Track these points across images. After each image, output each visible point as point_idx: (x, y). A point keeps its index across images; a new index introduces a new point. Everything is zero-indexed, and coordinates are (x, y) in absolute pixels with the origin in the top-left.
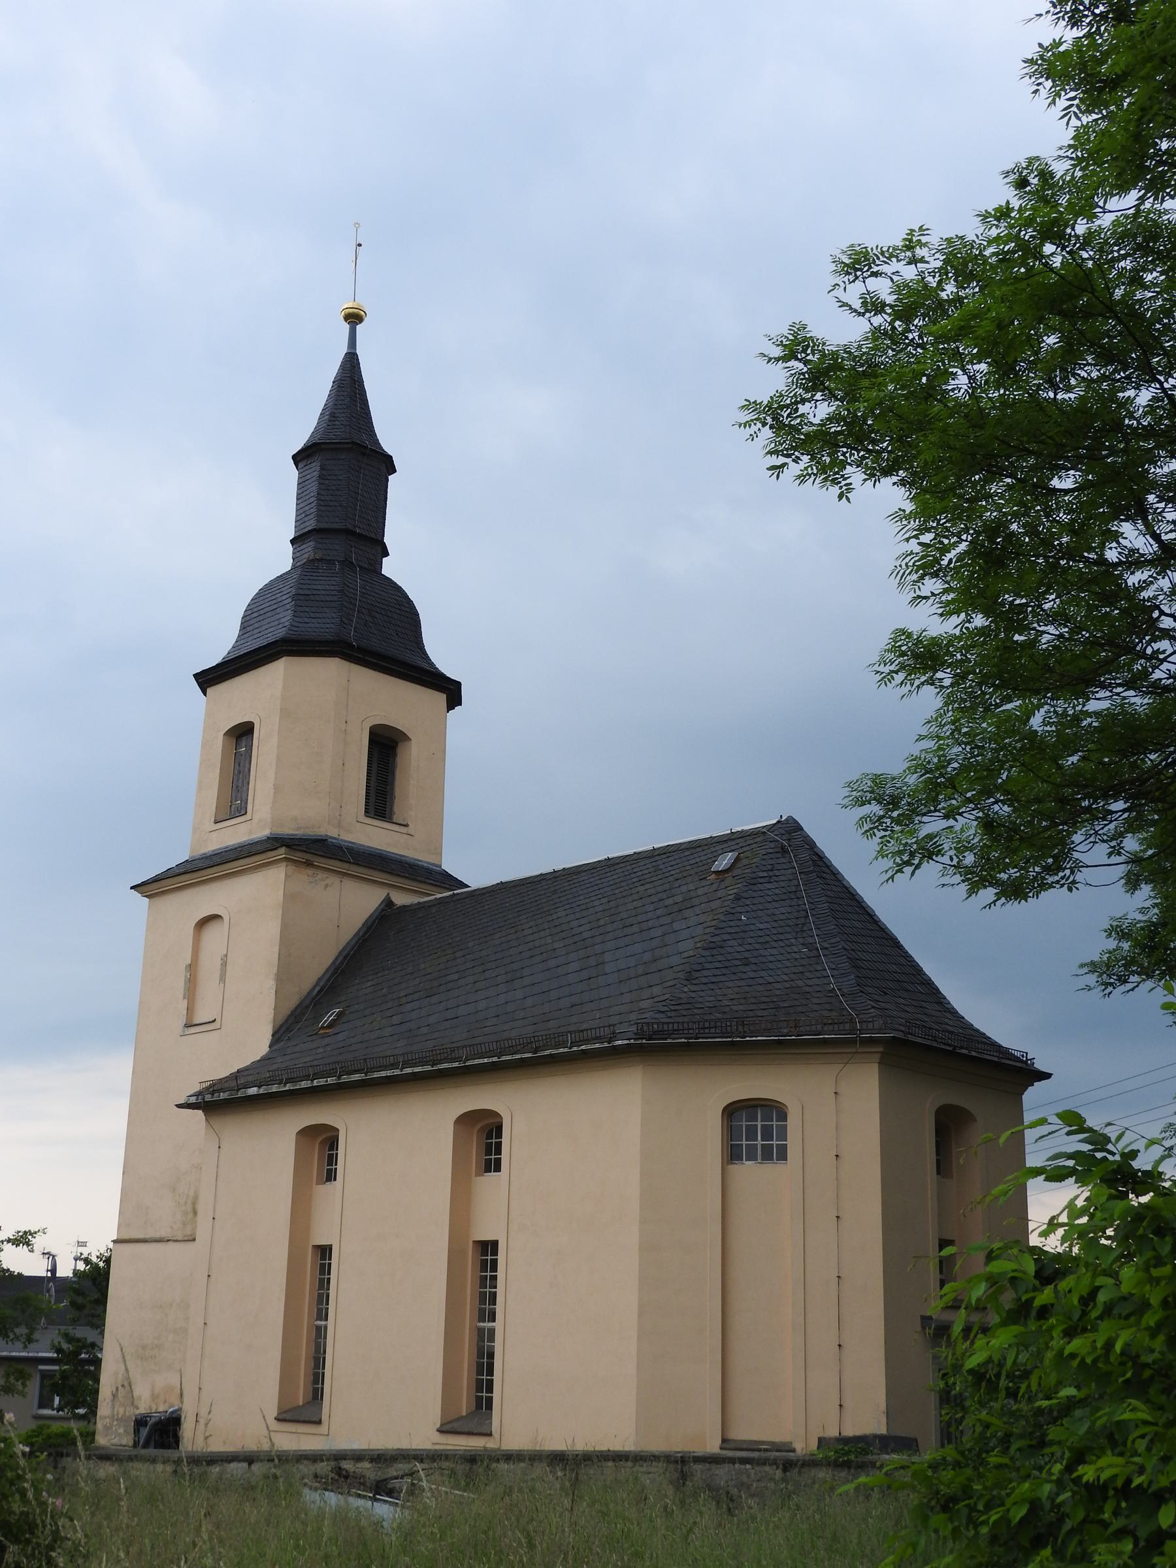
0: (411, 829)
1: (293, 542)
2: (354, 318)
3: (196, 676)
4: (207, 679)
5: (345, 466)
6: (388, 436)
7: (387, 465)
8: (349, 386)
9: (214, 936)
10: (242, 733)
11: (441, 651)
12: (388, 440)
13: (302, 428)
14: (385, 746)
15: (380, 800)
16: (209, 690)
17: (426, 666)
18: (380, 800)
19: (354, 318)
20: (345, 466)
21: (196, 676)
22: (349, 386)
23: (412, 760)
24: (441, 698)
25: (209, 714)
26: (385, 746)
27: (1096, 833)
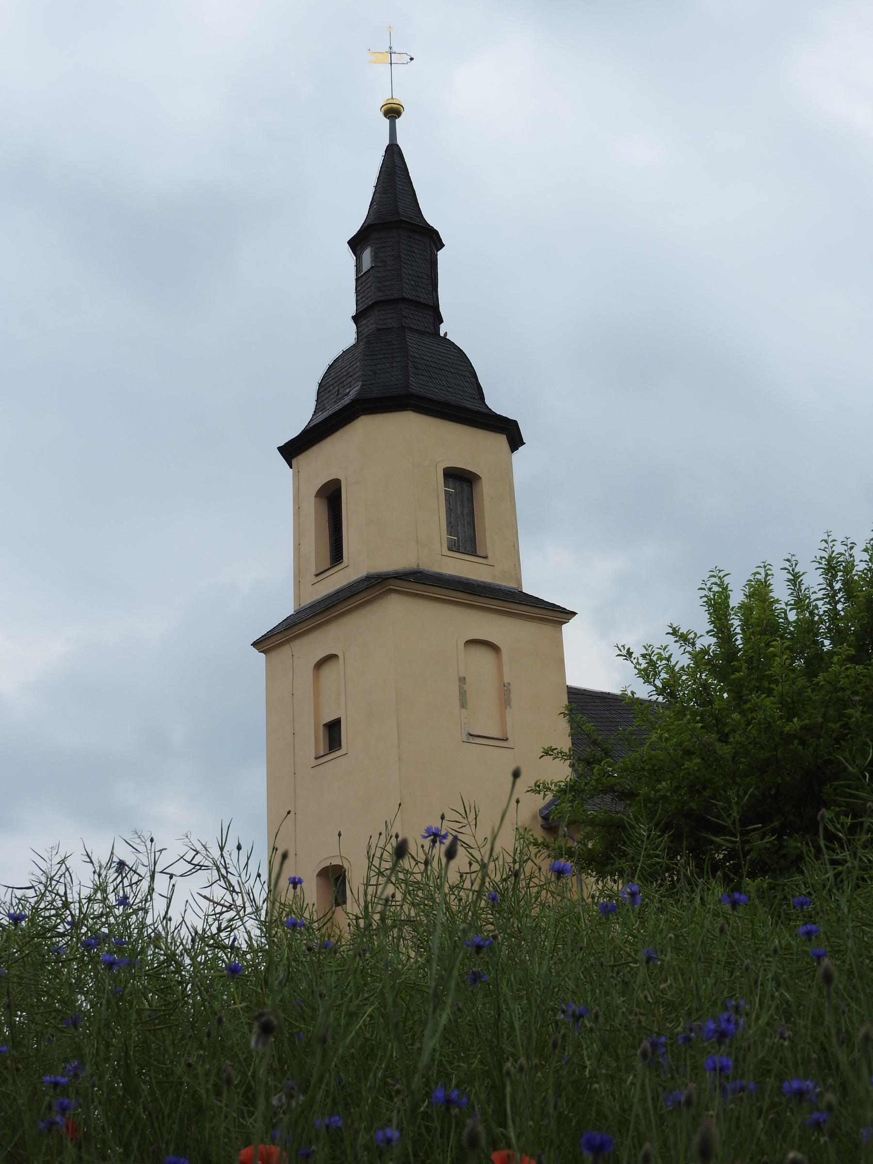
0: (490, 561)
1: (356, 319)
2: (393, 113)
3: (281, 449)
4: (291, 451)
5: (397, 241)
6: (432, 213)
7: (433, 240)
8: (394, 171)
9: (329, 672)
10: (331, 496)
11: (497, 402)
12: (432, 215)
13: (356, 216)
14: (461, 481)
15: (464, 532)
16: (294, 462)
17: (484, 410)
18: (464, 532)
19: (393, 113)
20: (397, 241)
21: (281, 449)
22: (394, 171)
23: (487, 490)
24: (501, 441)
25: (296, 477)
26: (461, 481)
27: (107, 1059)
